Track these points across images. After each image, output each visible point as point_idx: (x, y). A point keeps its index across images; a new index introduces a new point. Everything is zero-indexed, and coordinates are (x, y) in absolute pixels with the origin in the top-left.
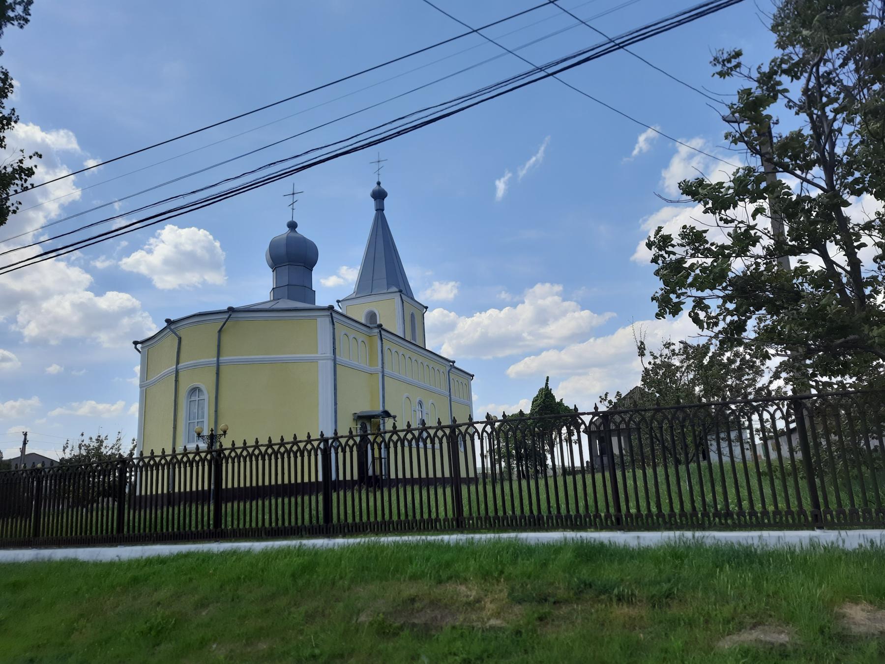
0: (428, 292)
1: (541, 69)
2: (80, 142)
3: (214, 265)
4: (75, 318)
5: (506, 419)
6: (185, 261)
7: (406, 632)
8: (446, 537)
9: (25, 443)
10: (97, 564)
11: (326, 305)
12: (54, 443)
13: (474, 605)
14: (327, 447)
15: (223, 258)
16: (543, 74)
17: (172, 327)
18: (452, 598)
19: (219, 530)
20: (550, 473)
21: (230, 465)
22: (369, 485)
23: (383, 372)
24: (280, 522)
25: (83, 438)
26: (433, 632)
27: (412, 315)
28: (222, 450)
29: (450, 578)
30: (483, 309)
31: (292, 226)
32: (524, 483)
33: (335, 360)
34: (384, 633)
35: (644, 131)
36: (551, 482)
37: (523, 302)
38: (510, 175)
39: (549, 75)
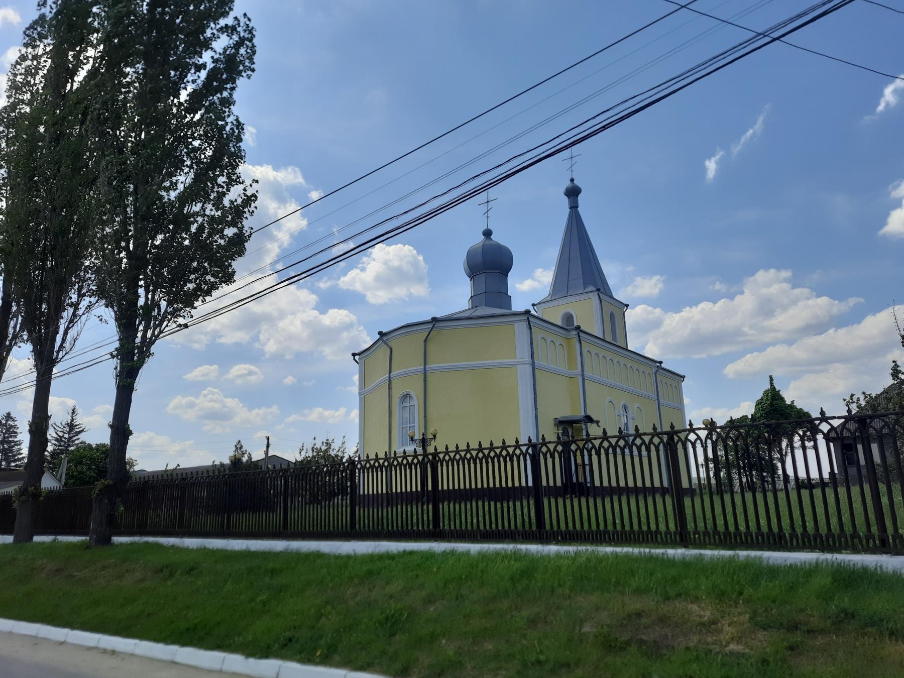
0: (629, 289)
1: (764, 34)
2: (305, 177)
3: (419, 279)
4: (305, 335)
5: (732, 424)
6: (393, 276)
7: (633, 648)
8: (671, 552)
9: (268, 447)
10: (338, 557)
11: (523, 309)
12: (290, 445)
13: (710, 626)
14: (535, 450)
15: (426, 271)
16: (768, 39)
17: (384, 339)
18: (683, 616)
19: (437, 530)
20: (780, 484)
21: (445, 468)
22: (573, 492)
23: (583, 375)
24: (494, 526)
25: (315, 442)
26: (664, 651)
27: (612, 315)
28: (436, 454)
29: (679, 595)
30: (694, 302)
31: (488, 233)
32: (749, 496)
33: (533, 364)
34: (610, 646)
35: (891, 82)
36: (782, 496)
37: (742, 293)
38: (722, 153)
39: (774, 40)
